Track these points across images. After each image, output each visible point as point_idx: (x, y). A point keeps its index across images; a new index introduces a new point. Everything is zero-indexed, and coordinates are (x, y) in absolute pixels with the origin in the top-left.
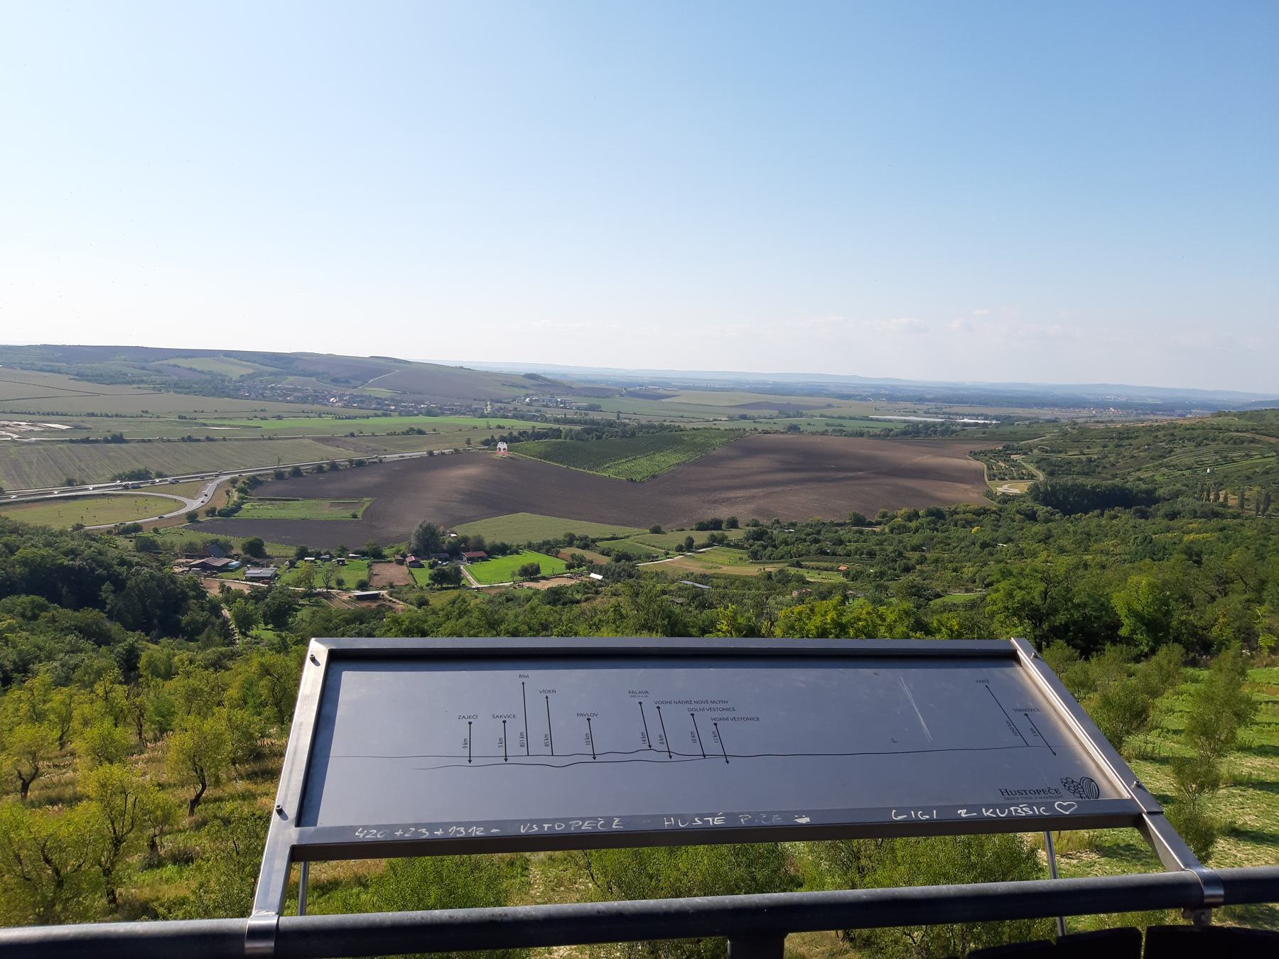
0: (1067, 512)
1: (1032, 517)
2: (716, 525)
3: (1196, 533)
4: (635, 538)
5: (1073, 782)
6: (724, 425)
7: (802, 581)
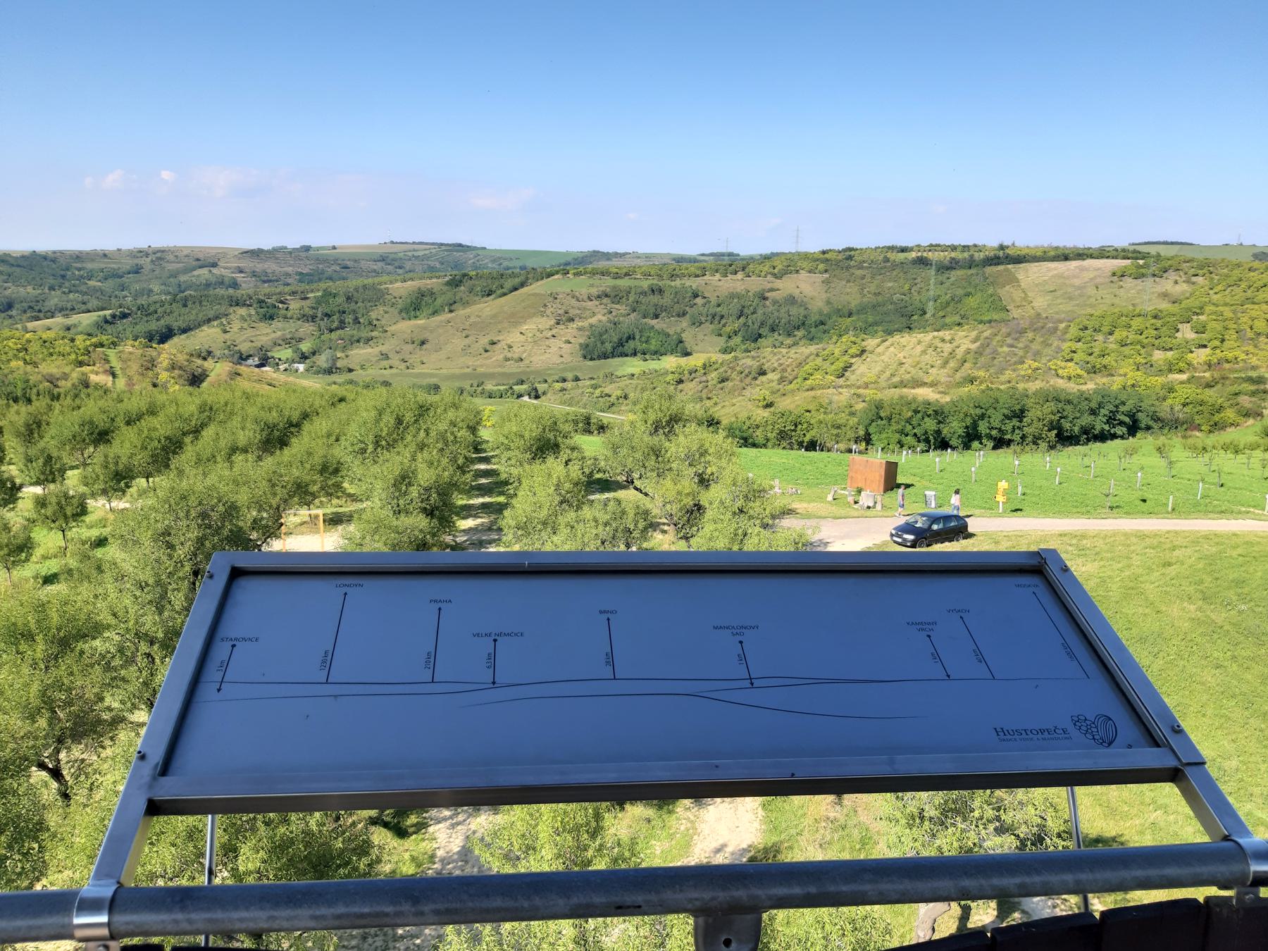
5: (1086, 719)
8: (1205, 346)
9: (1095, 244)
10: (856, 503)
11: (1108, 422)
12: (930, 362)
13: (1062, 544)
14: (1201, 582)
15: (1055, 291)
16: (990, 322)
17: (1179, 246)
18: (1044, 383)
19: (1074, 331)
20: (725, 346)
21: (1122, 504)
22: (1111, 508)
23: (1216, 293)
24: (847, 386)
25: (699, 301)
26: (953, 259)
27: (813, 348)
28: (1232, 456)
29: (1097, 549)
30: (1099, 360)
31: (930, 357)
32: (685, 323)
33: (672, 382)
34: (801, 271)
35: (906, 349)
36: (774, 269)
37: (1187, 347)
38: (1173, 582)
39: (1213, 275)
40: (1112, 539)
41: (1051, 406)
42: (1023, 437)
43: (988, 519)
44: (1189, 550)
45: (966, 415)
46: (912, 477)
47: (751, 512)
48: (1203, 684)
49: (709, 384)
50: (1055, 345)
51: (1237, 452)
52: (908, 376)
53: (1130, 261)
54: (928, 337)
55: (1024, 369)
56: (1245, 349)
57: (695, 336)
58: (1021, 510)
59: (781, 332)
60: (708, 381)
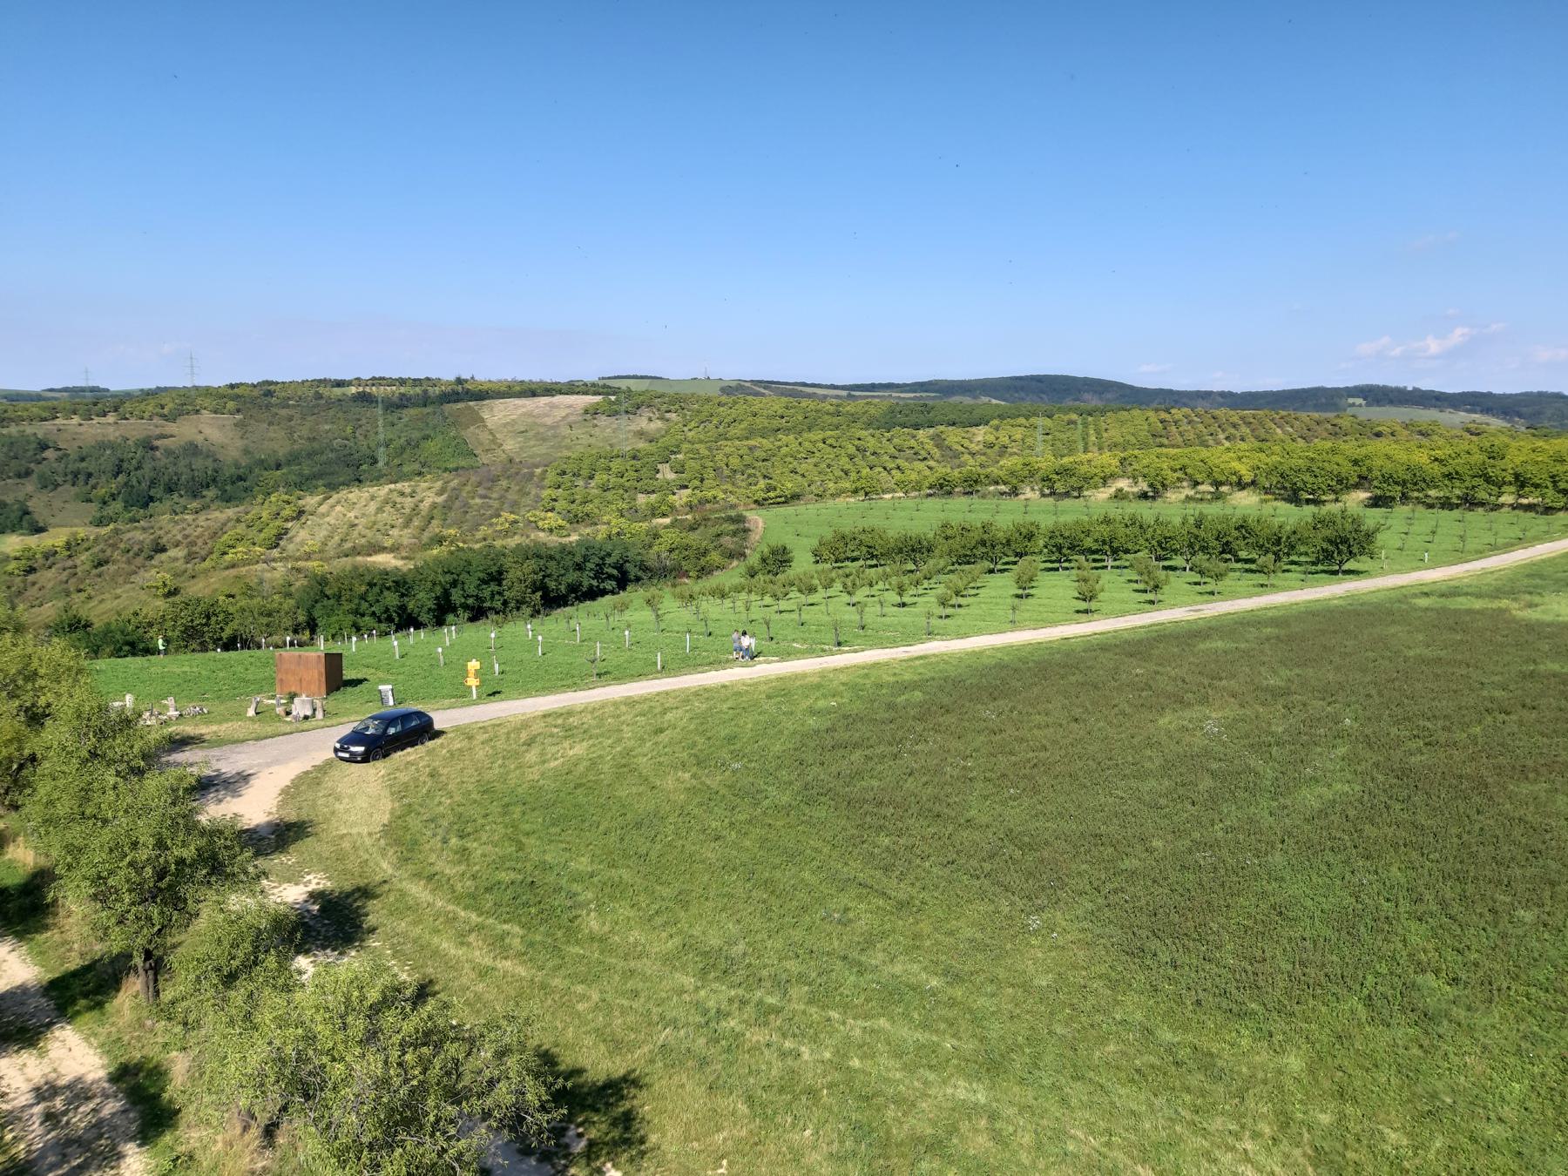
8: (686, 487)
9: (563, 378)
10: (288, 713)
11: (596, 577)
12: (389, 522)
13: (546, 726)
14: (694, 744)
15: (526, 431)
16: (456, 469)
17: (649, 380)
18: (524, 538)
19: (551, 477)
20: (98, 515)
21: (610, 669)
22: (599, 675)
23: (690, 430)
24: (286, 559)
25: (49, 454)
26: (403, 395)
27: (230, 512)
28: (719, 601)
29: (585, 726)
30: (580, 508)
31: (387, 516)
32: (30, 486)
33: (16, 572)
34: (203, 411)
35: (357, 506)
36: (163, 408)
37: (670, 489)
38: (666, 750)
39: (685, 411)
40: (601, 711)
41: (532, 565)
42: (505, 603)
43: (459, 710)
44: (680, 711)
45: (434, 584)
46: (365, 670)
47: (110, 754)
48: (703, 862)
49: (78, 570)
50: (533, 493)
51: (723, 596)
52: (363, 541)
53: (601, 397)
54: (384, 491)
55: (502, 521)
56: (724, 487)
57: (49, 505)
58: (499, 693)
59: (182, 493)
60: (76, 567)
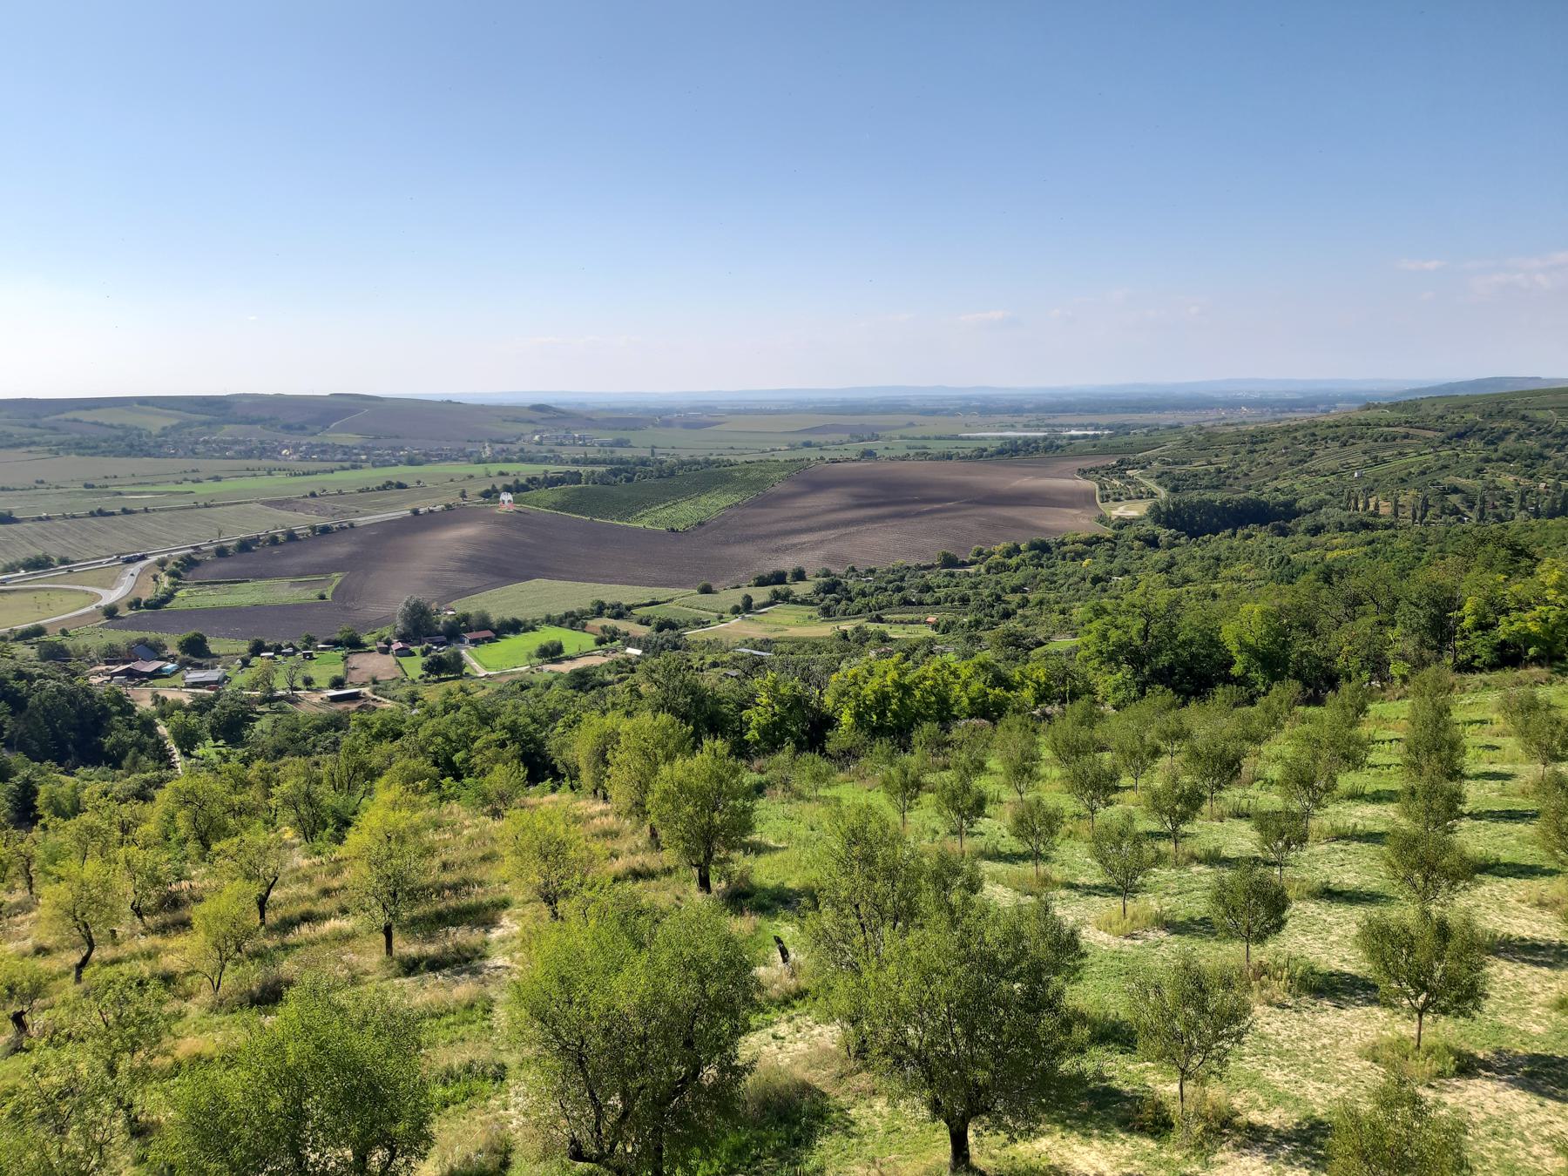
0: (1194, 534)
1: (1152, 542)
2: (779, 578)
3: (1340, 549)
4: (681, 601)
6: (782, 457)
7: (884, 639)
